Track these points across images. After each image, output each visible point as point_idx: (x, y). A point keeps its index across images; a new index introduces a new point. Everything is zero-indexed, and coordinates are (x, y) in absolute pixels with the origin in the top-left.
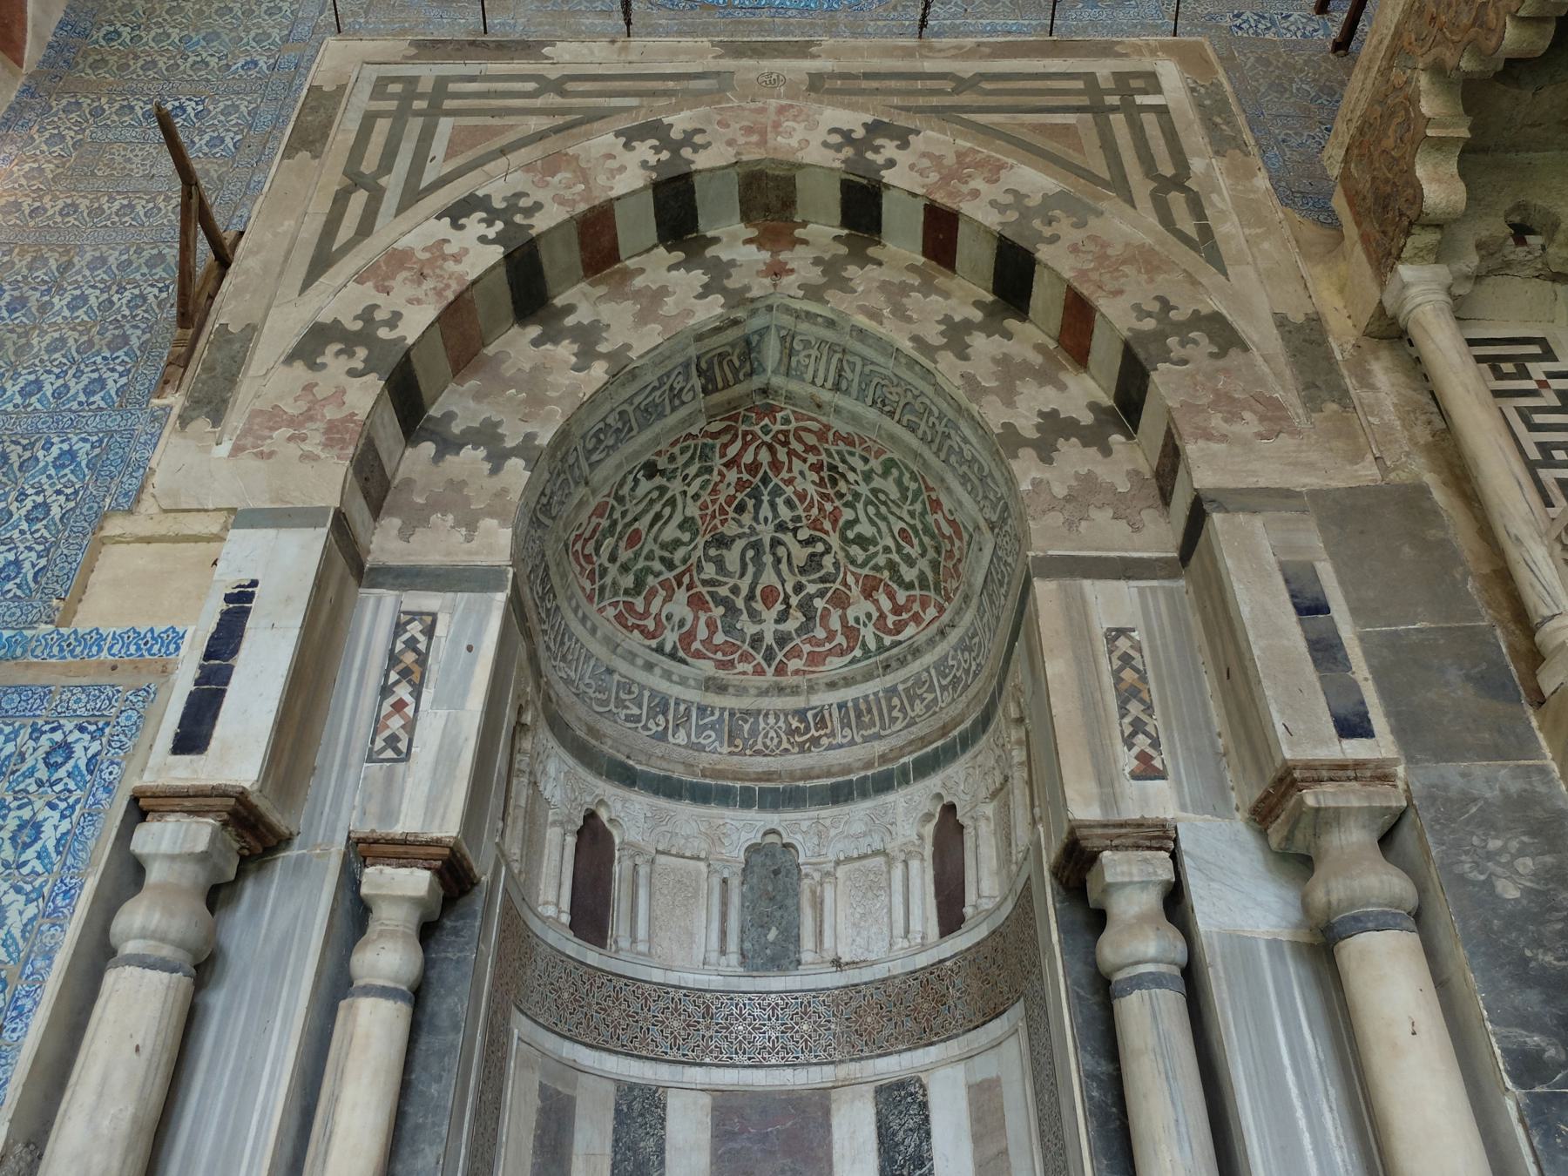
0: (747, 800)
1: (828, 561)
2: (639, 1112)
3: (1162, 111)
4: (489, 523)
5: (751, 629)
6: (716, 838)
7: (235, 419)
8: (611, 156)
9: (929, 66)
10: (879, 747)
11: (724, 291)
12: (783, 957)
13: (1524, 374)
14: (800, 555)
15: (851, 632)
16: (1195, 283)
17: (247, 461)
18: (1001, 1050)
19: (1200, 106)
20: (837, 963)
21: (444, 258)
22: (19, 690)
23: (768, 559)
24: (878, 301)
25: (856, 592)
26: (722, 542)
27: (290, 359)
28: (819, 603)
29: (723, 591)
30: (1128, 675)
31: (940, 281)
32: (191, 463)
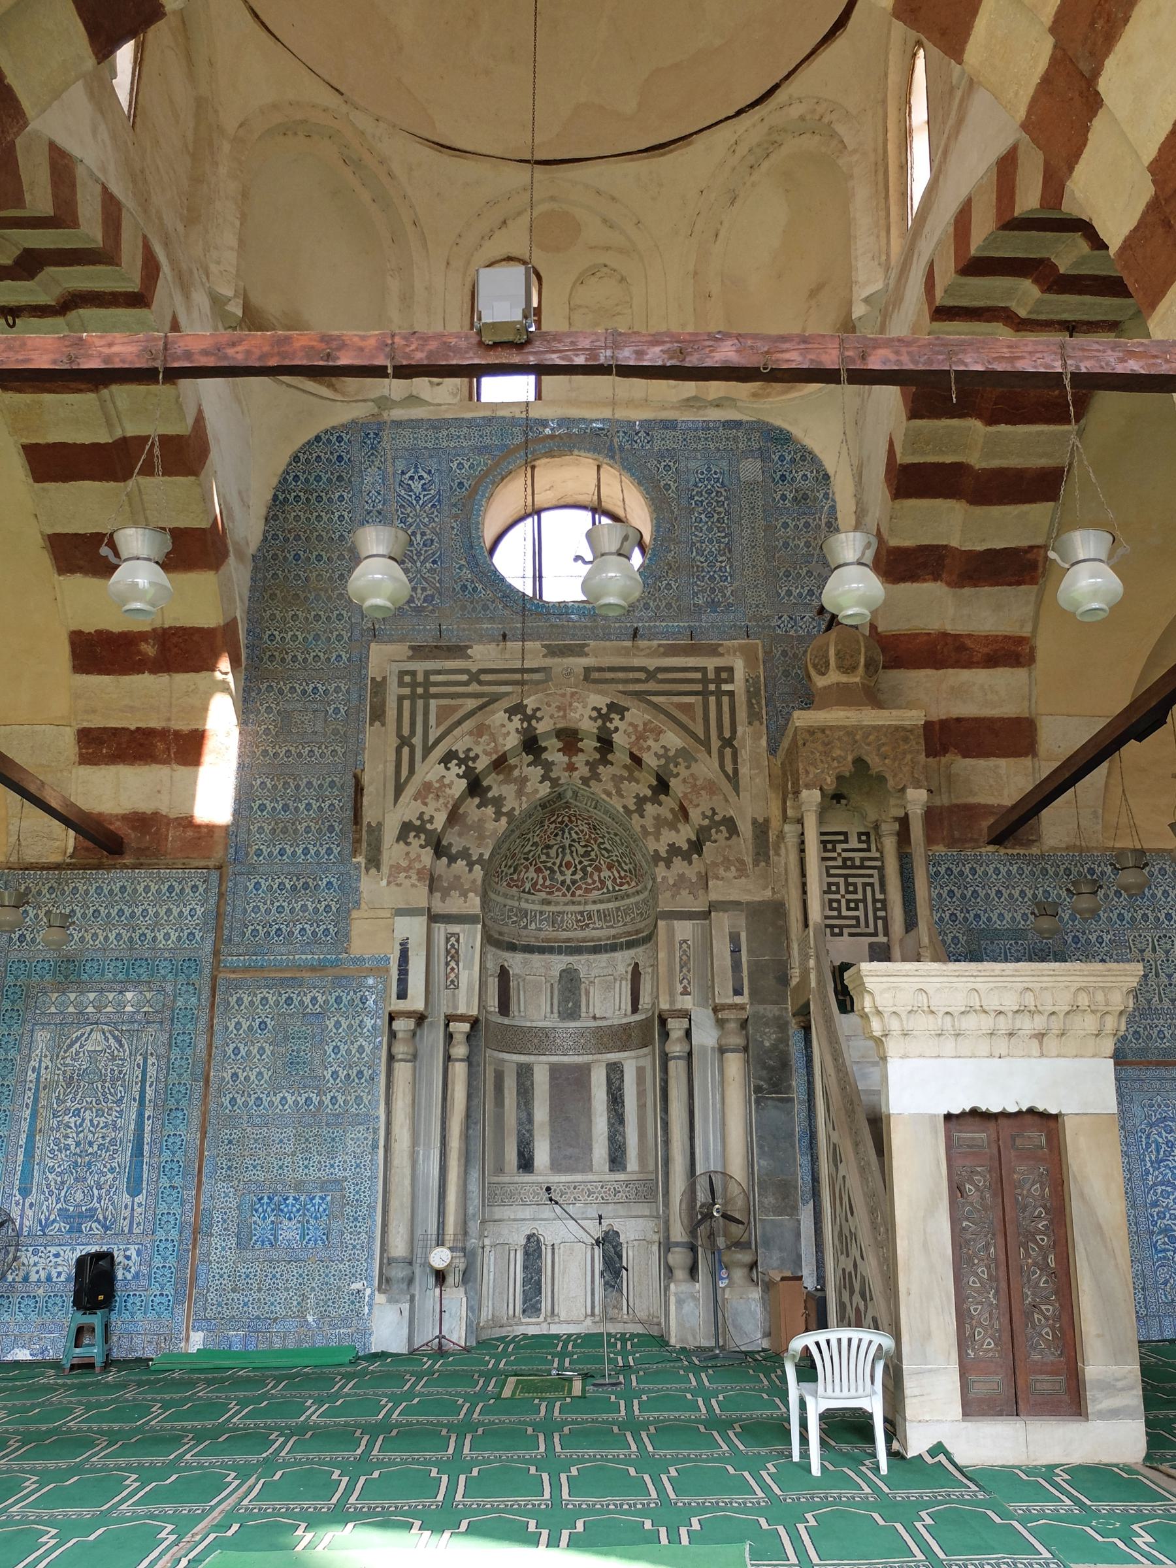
0: (560, 951)
1: (593, 854)
2: (524, 1073)
3: (731, 694)
4: (471, 895)
5: (561, 878)
6: (548, 967)
7: (385, 869)
8: (503, 726)
9: (636, 662)
10: (613, 932)
11: (550, 779)
12: (572, 1014)
13: (834, 850)
14: (581, 851)
15: (602, 882)
16: (727, 801)
17: (393, 887)
19: (748, 691)
20: (594, 1018)
21: (445, 786)
22: (345, 978)
23: (568, 851)
24: (610, 786)
25: (604, 867)
26: (549, 847)
27: (398, 841)
28: (589, 869)
29: (549, 865)
30: (684, 958)
31: (636, 773)
32: (374, 888)
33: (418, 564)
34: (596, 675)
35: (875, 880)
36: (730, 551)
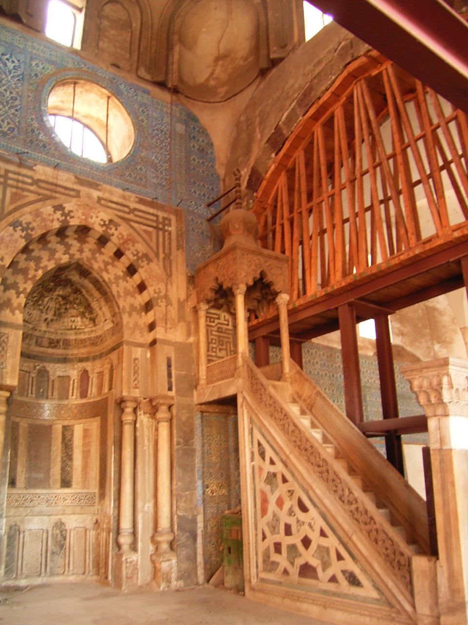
18: (94, 425)
33: (7, 108)
34: (103, 202)
35: (231, 340)
36: (170, 161)
